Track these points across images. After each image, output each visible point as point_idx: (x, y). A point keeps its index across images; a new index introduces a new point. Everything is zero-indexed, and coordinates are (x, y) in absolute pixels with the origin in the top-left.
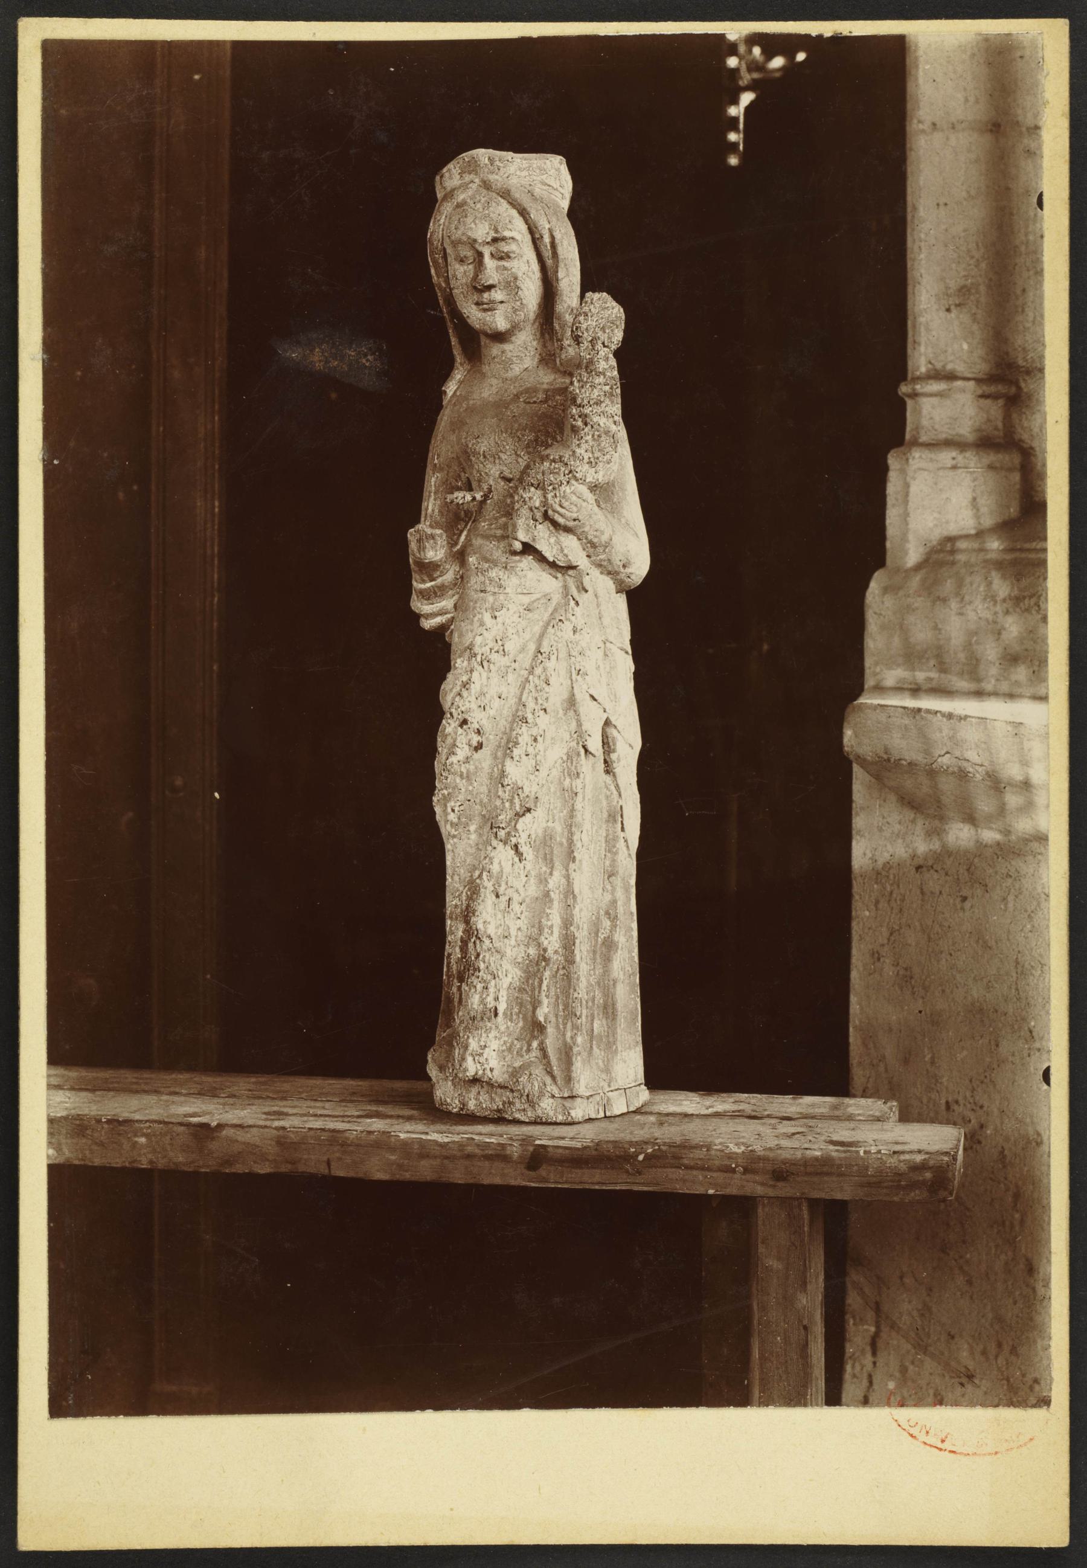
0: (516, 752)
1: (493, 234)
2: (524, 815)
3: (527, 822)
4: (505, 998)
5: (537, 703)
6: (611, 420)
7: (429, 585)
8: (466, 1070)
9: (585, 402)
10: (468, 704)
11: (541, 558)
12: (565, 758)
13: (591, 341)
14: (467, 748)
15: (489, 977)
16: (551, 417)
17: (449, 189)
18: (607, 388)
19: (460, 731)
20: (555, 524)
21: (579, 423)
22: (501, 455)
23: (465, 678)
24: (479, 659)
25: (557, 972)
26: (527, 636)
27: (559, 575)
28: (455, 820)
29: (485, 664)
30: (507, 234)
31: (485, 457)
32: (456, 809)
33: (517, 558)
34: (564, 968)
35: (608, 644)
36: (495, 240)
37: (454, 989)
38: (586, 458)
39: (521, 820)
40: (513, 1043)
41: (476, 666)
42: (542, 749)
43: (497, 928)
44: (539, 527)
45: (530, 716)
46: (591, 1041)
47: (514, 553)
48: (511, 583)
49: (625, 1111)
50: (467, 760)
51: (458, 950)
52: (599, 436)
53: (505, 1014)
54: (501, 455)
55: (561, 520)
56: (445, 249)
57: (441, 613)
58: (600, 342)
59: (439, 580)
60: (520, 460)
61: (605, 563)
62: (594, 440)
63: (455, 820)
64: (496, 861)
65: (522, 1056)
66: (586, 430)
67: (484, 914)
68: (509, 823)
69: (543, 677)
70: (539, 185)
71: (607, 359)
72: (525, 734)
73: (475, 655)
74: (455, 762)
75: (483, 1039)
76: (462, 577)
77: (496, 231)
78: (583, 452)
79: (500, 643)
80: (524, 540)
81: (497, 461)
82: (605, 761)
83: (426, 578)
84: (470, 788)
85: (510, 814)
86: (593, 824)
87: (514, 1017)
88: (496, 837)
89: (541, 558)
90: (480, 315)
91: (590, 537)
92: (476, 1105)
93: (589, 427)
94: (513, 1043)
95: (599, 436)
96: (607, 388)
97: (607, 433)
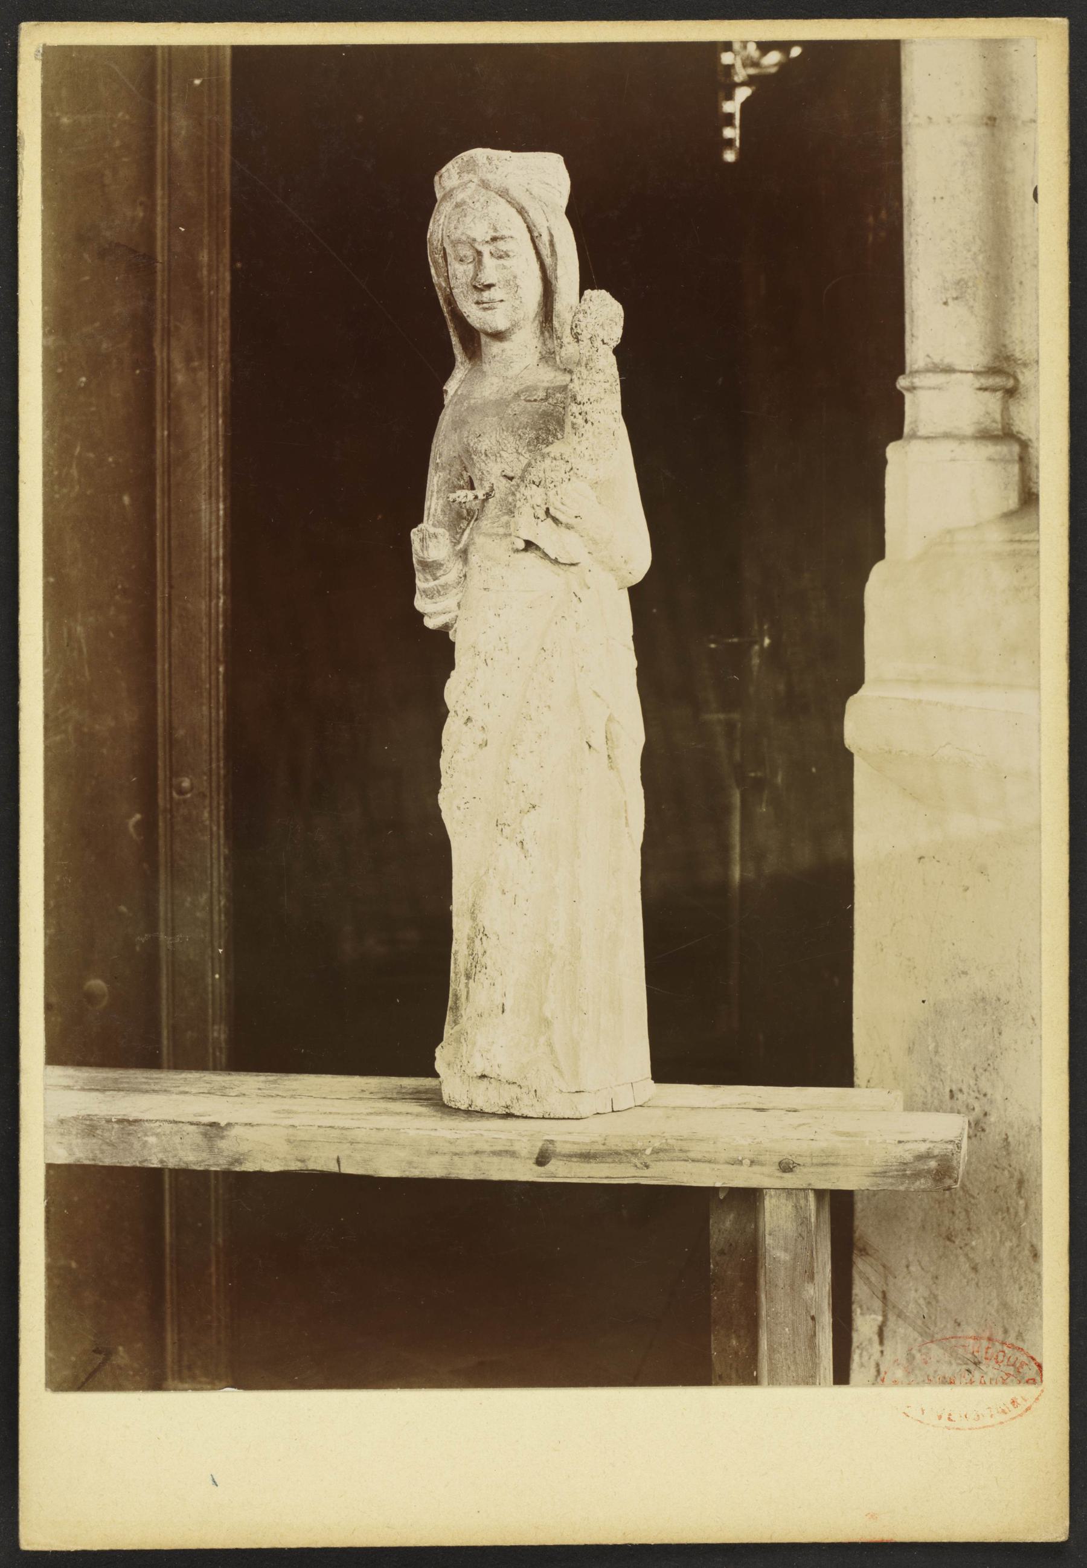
1: (492, 234)
17: (448, 189)
22: (502, 453)
24: (483, 658)
36: (494, 239)
54: (502, 453)
56: (444, 249)
77: (495, 230)
81: (499, 460)
83: (429, 577)
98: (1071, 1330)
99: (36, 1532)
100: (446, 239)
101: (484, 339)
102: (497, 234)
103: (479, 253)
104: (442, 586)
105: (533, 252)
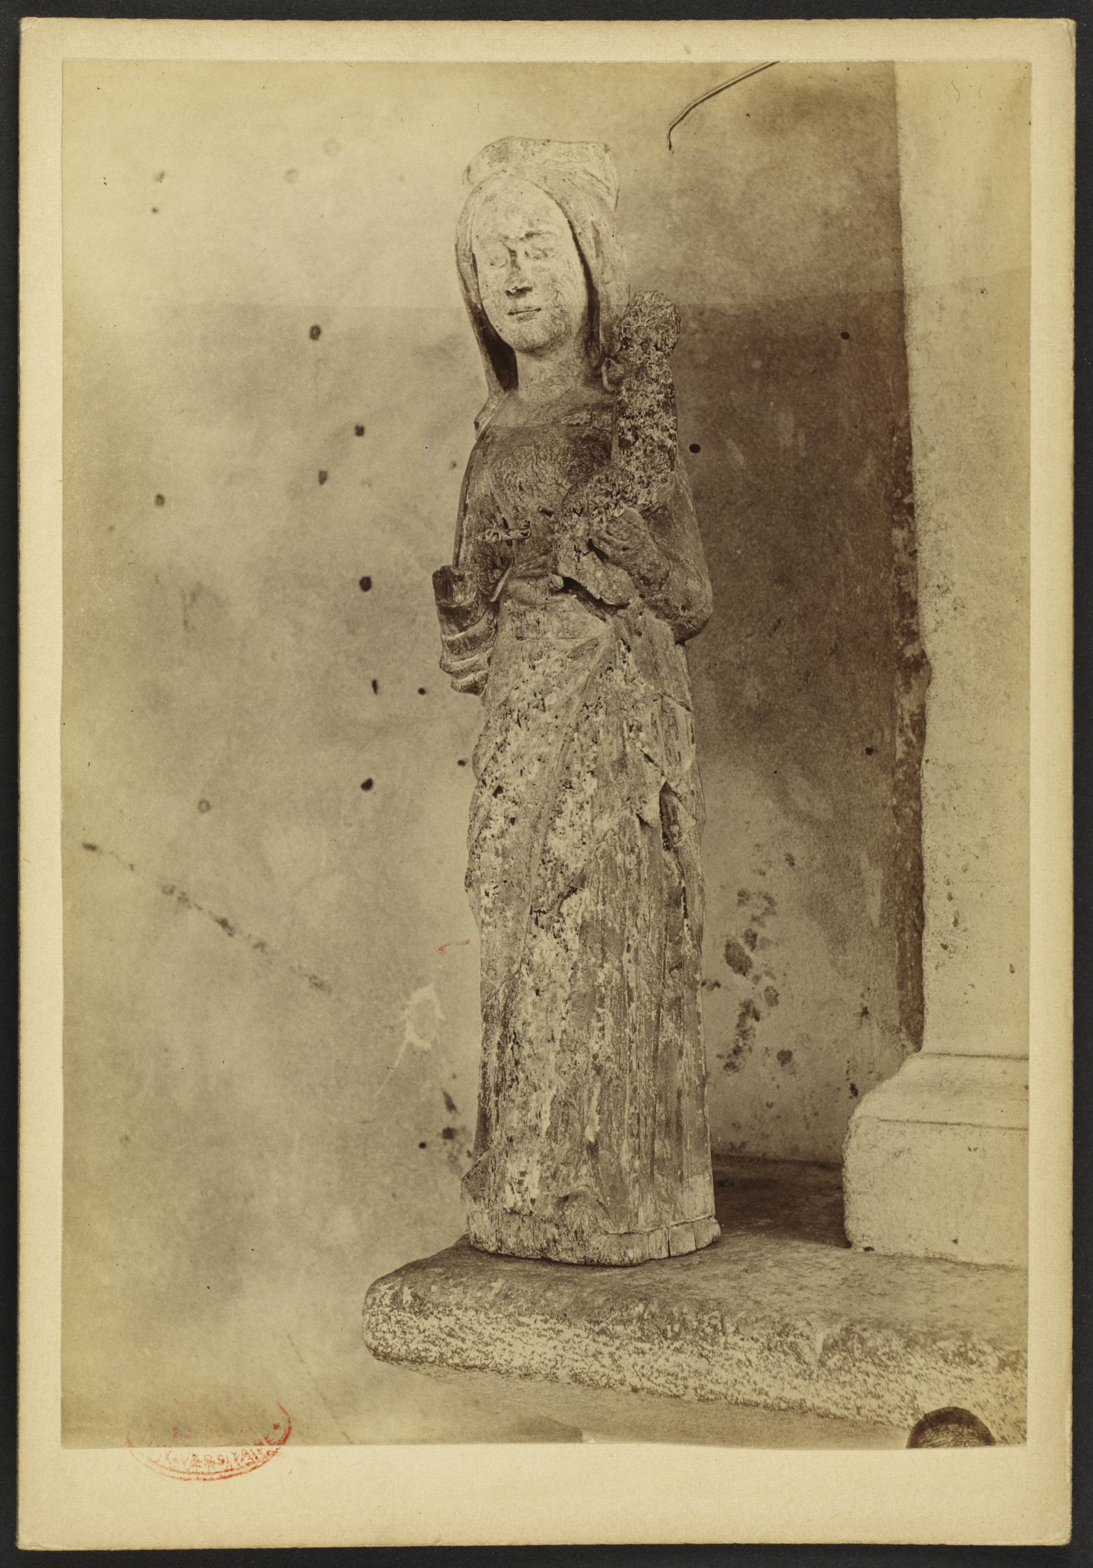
0: (559, 823)
1: (527, 229)
2: (568, 896)
3: (573, 904)
4: (548, 1115)
5: (583, 764)
6: (666, 434)
7: (459, 635)
8: (503, 1201)
9: (636, 413)
10: (503, 770)
11: (586, 597)
12: (616, 828)
13: (641, 345)
14: (502, 820)
15: (530, 1089)
16: (597, 440)
17: (477, 184)
18: (661, 396)
19: (495, 800)
20: (602, 556)
21: (630, 437)
22: (540, 485)
23: (499, 739)
24: (515, 717)
25: (609, 1083)
26: (570, 688)
27: (607, 616)
28: (490, 905)
29: (522, 721)
30: (543, 227)
31: (521, 489)
32: (491, 892)
33: (559, 597)
34: (618, 1078)
35: (666, 698)
36: (529, 235)
37: (492, 1105)
38: (637, 476)
39: (565, 902)
40: (558, 1168)
41: (512, 724)
42: (589, 817)
43: (538, 1030)
44: (583, 559)
45: (575, 780)
46: (652, 1165)
47: (554, 592)
48: (552, 625)
49: (693, 1248)
50: (502, 834)
51: (494, 1058)
52: (652, 451)
53: (547, 1133)
54: (540, 485)
55: (608, 550)
56: (473, 255)
57: (472, 669)
58: (652, 345)
59: (471, 631)
60: (561, 490)
61: (661, 604)
62: (646, 456)
63: (490, 905)
64: (537, 951)
65: (569, 1184)
66: (637, 444)
67: (523, 1013)
68: (552, 908)
69: (589, 734)
70: (581, 174)
71: (660, 365)
72: (570, 800)
73: (511, 711)
74: (489, 836)
75: (523, 1164)
76: (496, 627)
77: (531, 224)
78: (633, 470)
79: (539, 697)
80: (567, 575)
81: (536, 493)
82: (665, 836)
83: (453, 627)
84: (507, 867)
85: (553, 895)
86: (650, 908)
87: (560, 1137)
88: (537, 923)
89: (586, 597)
90: (515, 326)
91: (642, 572)
92: (516, 1243)
93: (640, 440)
94: (558, 1168)
95: (652, 451)
96: (661, 396)
97: (662, 447)
98: (412, 19)
99: (32, 1535)
100: (475, 241)
101: (521, 359)
102: (533, 230)
103: (513, 253)
104: (469, 639)
105: (576, 253)
